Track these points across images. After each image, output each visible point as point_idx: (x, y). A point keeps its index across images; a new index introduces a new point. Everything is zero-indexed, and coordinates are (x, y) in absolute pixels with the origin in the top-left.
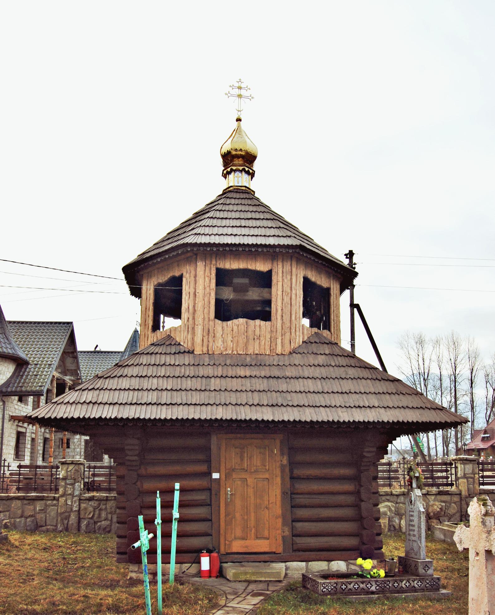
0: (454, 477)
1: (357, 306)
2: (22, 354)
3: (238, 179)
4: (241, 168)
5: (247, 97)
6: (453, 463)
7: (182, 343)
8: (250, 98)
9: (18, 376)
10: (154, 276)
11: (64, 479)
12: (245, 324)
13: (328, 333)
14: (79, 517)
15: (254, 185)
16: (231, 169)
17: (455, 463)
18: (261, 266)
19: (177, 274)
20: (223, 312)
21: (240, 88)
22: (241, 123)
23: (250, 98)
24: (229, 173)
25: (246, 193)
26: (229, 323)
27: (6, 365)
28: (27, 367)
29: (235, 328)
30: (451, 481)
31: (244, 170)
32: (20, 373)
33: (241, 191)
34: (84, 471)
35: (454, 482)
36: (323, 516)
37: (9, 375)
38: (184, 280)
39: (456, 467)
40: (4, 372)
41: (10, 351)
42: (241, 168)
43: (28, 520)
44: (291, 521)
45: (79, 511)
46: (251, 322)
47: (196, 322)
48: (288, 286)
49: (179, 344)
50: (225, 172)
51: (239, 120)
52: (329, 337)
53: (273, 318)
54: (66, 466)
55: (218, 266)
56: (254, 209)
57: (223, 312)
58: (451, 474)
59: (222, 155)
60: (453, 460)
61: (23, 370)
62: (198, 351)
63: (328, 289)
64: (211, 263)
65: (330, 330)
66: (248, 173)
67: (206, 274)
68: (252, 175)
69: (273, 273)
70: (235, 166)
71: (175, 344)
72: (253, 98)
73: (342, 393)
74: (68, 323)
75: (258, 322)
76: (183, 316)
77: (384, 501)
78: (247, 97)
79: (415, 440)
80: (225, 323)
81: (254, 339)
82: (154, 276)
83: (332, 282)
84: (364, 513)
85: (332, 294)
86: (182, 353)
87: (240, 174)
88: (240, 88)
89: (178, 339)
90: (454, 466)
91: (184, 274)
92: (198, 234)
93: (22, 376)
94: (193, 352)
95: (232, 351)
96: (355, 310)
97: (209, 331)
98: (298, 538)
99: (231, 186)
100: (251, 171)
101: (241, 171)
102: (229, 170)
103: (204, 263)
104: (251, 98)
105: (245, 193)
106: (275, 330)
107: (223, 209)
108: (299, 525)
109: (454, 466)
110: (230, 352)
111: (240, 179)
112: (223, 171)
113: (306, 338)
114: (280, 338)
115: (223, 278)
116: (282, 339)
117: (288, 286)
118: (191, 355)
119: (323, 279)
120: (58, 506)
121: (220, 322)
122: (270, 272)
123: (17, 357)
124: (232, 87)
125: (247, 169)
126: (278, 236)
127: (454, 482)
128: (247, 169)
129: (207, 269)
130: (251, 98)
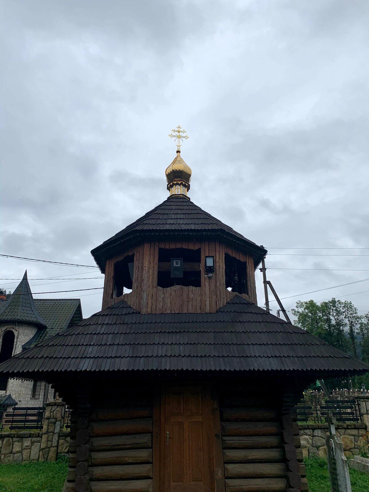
0: (358, 413)
1: (269, 283)
2: (43, 322)
3: (178, 190)
4: (180, 182)
5: (184, 137)
6: (356, 400)
7: (132, 306)
8: (186, 137)
9: (38, 337)
10: (115, 256)
11: (48, 418)
12: (181, 290)
13: (247, 296)
14: (57, 451)
15: (188, 194)
16: (173, 184)
17: (358, 401)
18: (193, 247)
19: (130, 254)
20: (165, 280)
21: (179, 132)
22: (177, 150)
23: (186, 137)
24: (172, 186)
25: (185, 200)
26: (168, 289)
27: (30, 329)
28: (45, 331)
29: (173, 293)
30: (356, 416)
31: (182, 183)
32: (40, 334)
33: (180, 197)
34: (65, 411)
35: (359, 418)
36: (250, 458)
37: (31, 337)
38: (135, 258)
39: (359, 405)
40: (28, 334)
41: (33, 319)
42: (180, 182)
43: (15, 455)
44: (223, 463)
45: (57, 447)
46: (185, 288)
47: (144, 289)
48: (214, 259)
49: (130, 307)
50: (169, 186)
51: (178, 152)
52: (247, 299)
53: (202, 285)
54: (50, 407)
55: (160, 247)
56: (188, 208)
57: (165, 280)
58: (356, 410)
59: (166, 175)
60: (356, 398)
61: (42, 332)
62: (144, 311)
63: (245, 263)
64: (155, 245)
65: (248, 294)
66: (185, 186)
67: (151, 253)
68: (188, 188)
69: (202, 251)
70: (176, 181)
71: (127, 307)
72: (188, 137)
73: (260, 344)
74: (77, 300)
75: (191, 288)
76: (133, 285)
77: (303, 435)
78: (184, 137)
79: (358, 432)
80: (165, 289)
81: (188, 301)
82: (115, 256)
83: (247, 258)
84: (288, 456)
85: (248, 267)
86: (131, 314)
87: (179, 187)
88: (179, 132)
89: (129, 303)
90: (357, 403)
91: (135, 253)
92: (145, 224)
93: (41, 337)
94: (140, 313)
95: (171, 311)
96: (268, 285)
97: (153, 296)
98: (230, 480)
99: (173, 195)
100: (187, 185)
101: (180, 185)
102: (171, 184)
103: (150, 245)
104: (186, 137)
105: (183, 198)
106: (204, 294)
107: (166, 208)
108: (230, 467)
109: (357, 403)
110: (169, 312)
111: (179, 190)
112: (168, 185)
113: (229, 300)
114: (208, 300)
115: (165, 256)
116: (210, 301)
117: (214, 259)
118: (139, 315)
119: (240, 255)
120: (40, 442)
121: (161, 288)
122: (199, 250)
123: (39, 324)
124: (174, 131)
125: (184, 183)
126: (205, 224)
127: (359, 418)
128: (184, 183)
129: (152, 250)
130: (186, 137)
